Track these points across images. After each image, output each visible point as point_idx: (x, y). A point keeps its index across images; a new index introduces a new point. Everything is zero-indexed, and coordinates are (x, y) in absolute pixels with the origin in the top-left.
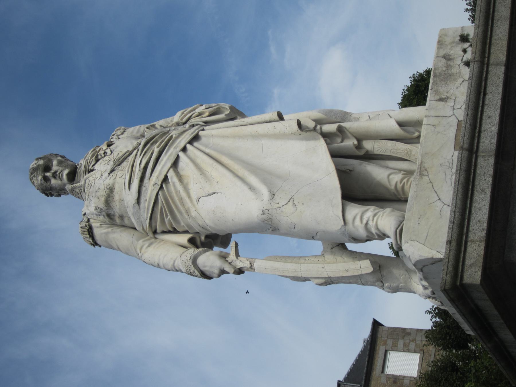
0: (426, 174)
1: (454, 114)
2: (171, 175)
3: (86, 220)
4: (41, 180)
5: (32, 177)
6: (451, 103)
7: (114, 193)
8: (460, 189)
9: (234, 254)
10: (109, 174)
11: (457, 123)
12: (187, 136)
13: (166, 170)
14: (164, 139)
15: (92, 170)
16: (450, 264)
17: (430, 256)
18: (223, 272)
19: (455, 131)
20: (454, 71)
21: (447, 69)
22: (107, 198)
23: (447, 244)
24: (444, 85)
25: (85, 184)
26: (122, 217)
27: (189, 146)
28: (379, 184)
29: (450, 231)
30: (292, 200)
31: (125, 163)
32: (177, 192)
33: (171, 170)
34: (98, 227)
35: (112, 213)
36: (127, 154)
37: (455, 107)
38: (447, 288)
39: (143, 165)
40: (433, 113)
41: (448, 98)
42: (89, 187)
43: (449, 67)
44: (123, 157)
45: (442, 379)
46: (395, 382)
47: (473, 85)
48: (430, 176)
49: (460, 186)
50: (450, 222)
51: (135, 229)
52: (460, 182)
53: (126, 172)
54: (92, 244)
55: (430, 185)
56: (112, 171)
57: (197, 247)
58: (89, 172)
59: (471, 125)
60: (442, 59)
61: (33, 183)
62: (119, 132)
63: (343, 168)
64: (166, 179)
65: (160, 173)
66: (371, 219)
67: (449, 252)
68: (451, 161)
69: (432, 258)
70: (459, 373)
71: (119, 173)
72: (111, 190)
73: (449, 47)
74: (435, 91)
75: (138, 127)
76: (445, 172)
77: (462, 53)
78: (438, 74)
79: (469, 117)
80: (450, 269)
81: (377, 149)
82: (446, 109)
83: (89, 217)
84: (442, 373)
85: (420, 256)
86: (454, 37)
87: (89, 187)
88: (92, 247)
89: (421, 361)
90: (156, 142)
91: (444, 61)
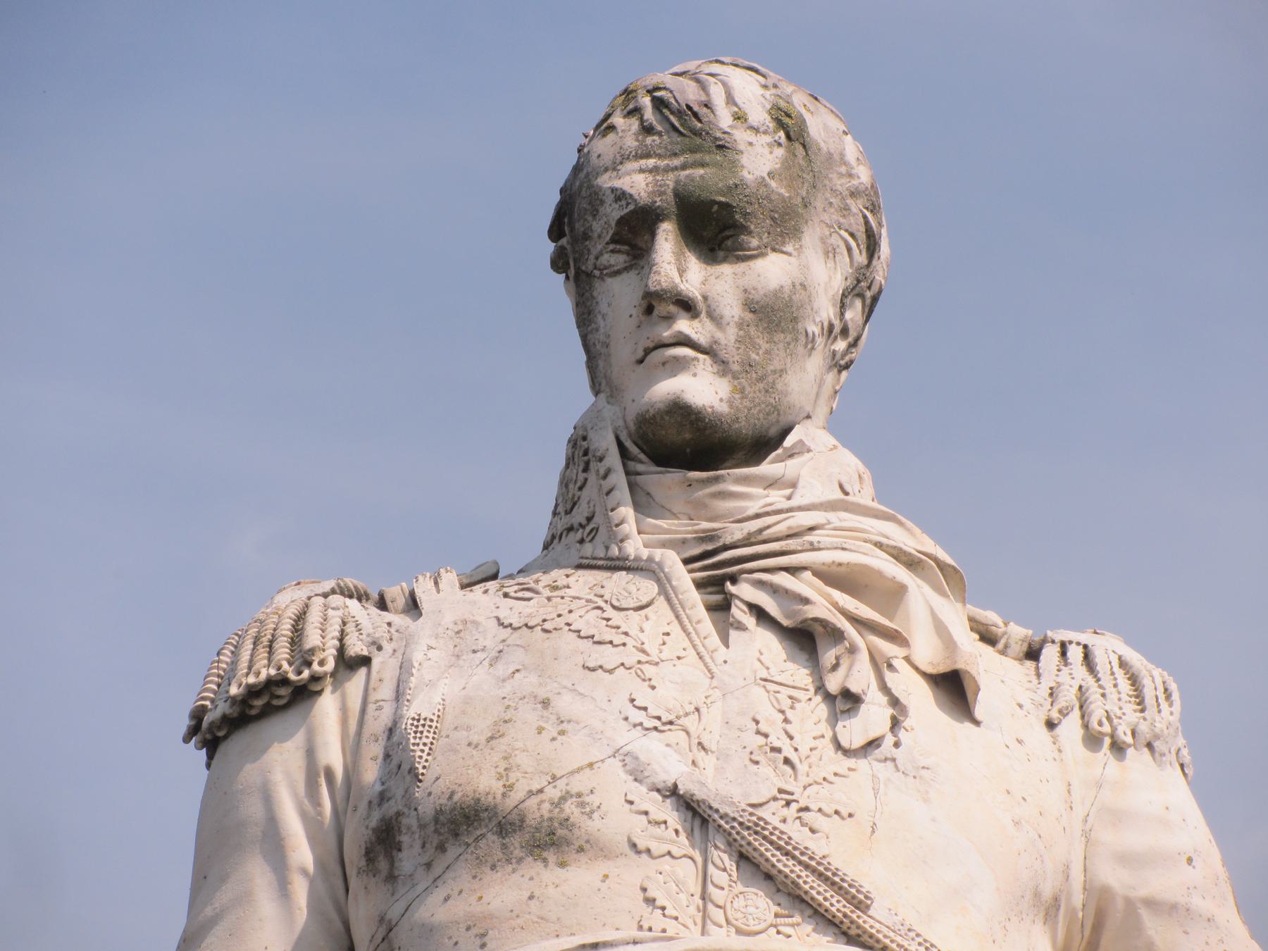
3: (356, 647)
5: (636, 111)
7: (531, 867)
10: (673, 792)
15: (721, 608)
22: (492, 810)
25: (617, 564)
34: (310, 753)
35: (408, 860)
36: (836, 905)
42: (588, 621)
44: (810, 884)
54: (198, 715)
56: (696, 814)
72: (551, 839)
83: (376, 663)
87: (588, 621)
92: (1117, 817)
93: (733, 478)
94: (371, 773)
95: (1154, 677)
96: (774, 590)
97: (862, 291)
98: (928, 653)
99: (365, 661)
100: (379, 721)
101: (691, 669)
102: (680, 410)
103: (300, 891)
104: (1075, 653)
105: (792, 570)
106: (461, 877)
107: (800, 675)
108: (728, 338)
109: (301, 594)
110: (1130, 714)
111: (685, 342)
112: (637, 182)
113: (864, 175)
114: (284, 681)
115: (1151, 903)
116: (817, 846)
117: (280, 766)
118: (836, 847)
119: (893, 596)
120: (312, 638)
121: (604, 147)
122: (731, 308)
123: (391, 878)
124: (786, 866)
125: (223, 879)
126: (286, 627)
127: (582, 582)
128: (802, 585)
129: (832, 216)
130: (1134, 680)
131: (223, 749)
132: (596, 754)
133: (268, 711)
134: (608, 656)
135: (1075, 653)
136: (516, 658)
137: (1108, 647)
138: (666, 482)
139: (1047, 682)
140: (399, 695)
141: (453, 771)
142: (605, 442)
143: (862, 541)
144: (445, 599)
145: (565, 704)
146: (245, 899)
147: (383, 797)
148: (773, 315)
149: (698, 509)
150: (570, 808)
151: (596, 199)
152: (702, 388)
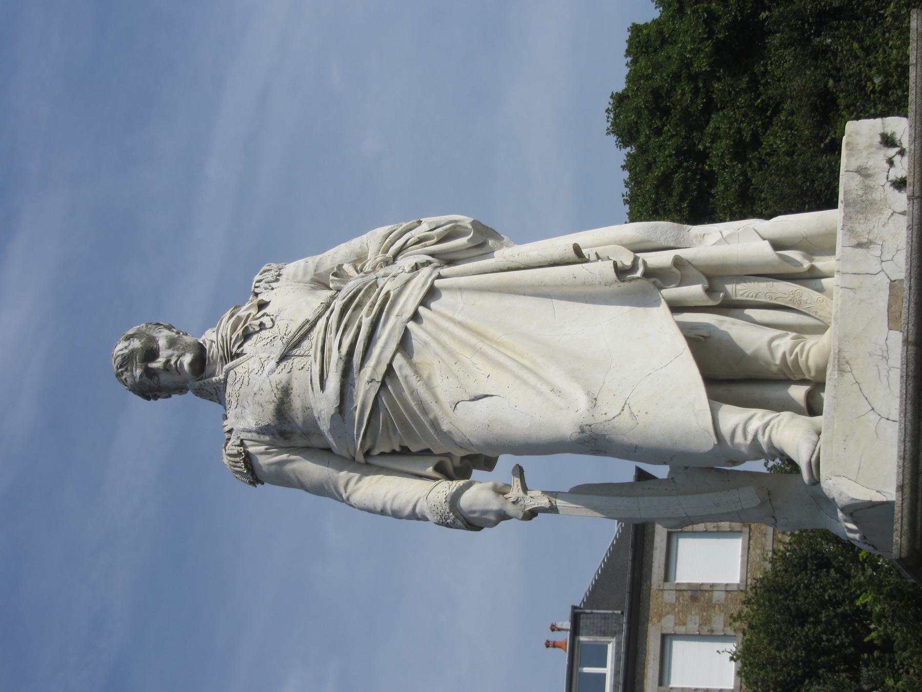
0: (849, 369)
1: (883, 270)
2: (399, 362)
3: (238, 442)
4: (141, 376)
5: (122, 372)
6: (876, 251)
8: (909, 407)
9: (520, 487)
10: (278, 363)
11: (888, 285)
12: (416, 292)
13: (390, 356)
14: (376, 300)
15: (238, 355)
16: (905, 519)
17: (867, 498)
18: (503, 516)
19: (886, 298)
20: (877, 195)
21: (866, 193)
23: (897, 491)
24: (862, 221)
26: (306, 435)
27: (422, 310)
28: (754, 359)
29: (901, 470)
30: (627, 406)
31: (306, 344)
32: (413, 392)
33: (399, 356)
34: (262, 453)
35: (288, 429)
36: (307, 326)
37: (884, 258)
38: (903, 555)
39: (344, 349)
40: (849, 268)
41: (870, 242)
42: (238, 386)
43: (868, 189)
44: (301, 332)
45: (799, 587)
46: (694, 599)
47: (914, 239)
48: (854, 372)
49: (909, 402)
50: (899, 457)
51: (329, 450)
52: (909, 396)
53: (312, 358)
54: (251, 483)
55: (856, 387)
57: (450, 478)
58: (232, 359)
59: (916, 304)
60: (856, 174)
61: (124, 382)
62: (269, 276)
63: (692, 334)
64: (390, 369)
65: (378, 362)
66: (760, 432)
67: (902, 504)
68: (885, 348)
69: (871, 501)
70: (832, 571)
71: (296, 362)
72: (286, 392)
73: (865, 154)
74: (849, 231)
75: (301, 262)
76: (877, 366)
77: (887, 166)
78: (851, 201)
79: (912, 291)
80: (905, 527)
81: (741, 293)
82: (868, 260)
84: (796, 575)
85: (853, 499)
86: (871, 137)
87: (238, 386)
88: (251, 487)
89: (747, 550)
90: (359, 306)
91: (858, 178)
92: (295, 276)
93: (209, 354)
94: (267, 438)
95: (265, 268)
96: (235, 343)
97: (170, 328)
98: (254, 311)
99: (242, 440)
100: (255, 436)
101: (251, 361)
102: (191, 364)
103: (293, 457)
104: (257, 284)
105: (231, 339)
106: (293, 414)
107: (255, 337)
108: (176, 353)
109: (225, 457)
110: (273, 272)
111: (176, 363)
112: (138, 372)
113: (143, 325)
114: (244, 459)
115: (315, 271)
116: (294, 330)
117: (264, 461)
118: (294, 328)
119: (239, 319)
120: (235, 452)
121: (129, 381)
122: (170, 352)
123: (292, 433)
124: (297, 337)
125: (288, 476)
126: (232, 459)
127: (229, 389)
128: (234, 337)
129: (151, 331)
130: (265, 272)
131: (260, 478)
132: (268, 381)
133: (251, 464)
134: (246, 380)
135: (257, 284)
136: (245, 403)
137: (258, 277)
138: (208, 370)
139: (263, 290)
140: (250, 431)
141: (267, 417)
142: (197, 384)
143: (226, 324)
144: (229, 424)
145: (255, 389)
146: (294, 471)
147: (273, 434)
148: (172, 343)
149: (215, 363)
150: (279, 387)
151: (141, 383)
152: (187, 359)
